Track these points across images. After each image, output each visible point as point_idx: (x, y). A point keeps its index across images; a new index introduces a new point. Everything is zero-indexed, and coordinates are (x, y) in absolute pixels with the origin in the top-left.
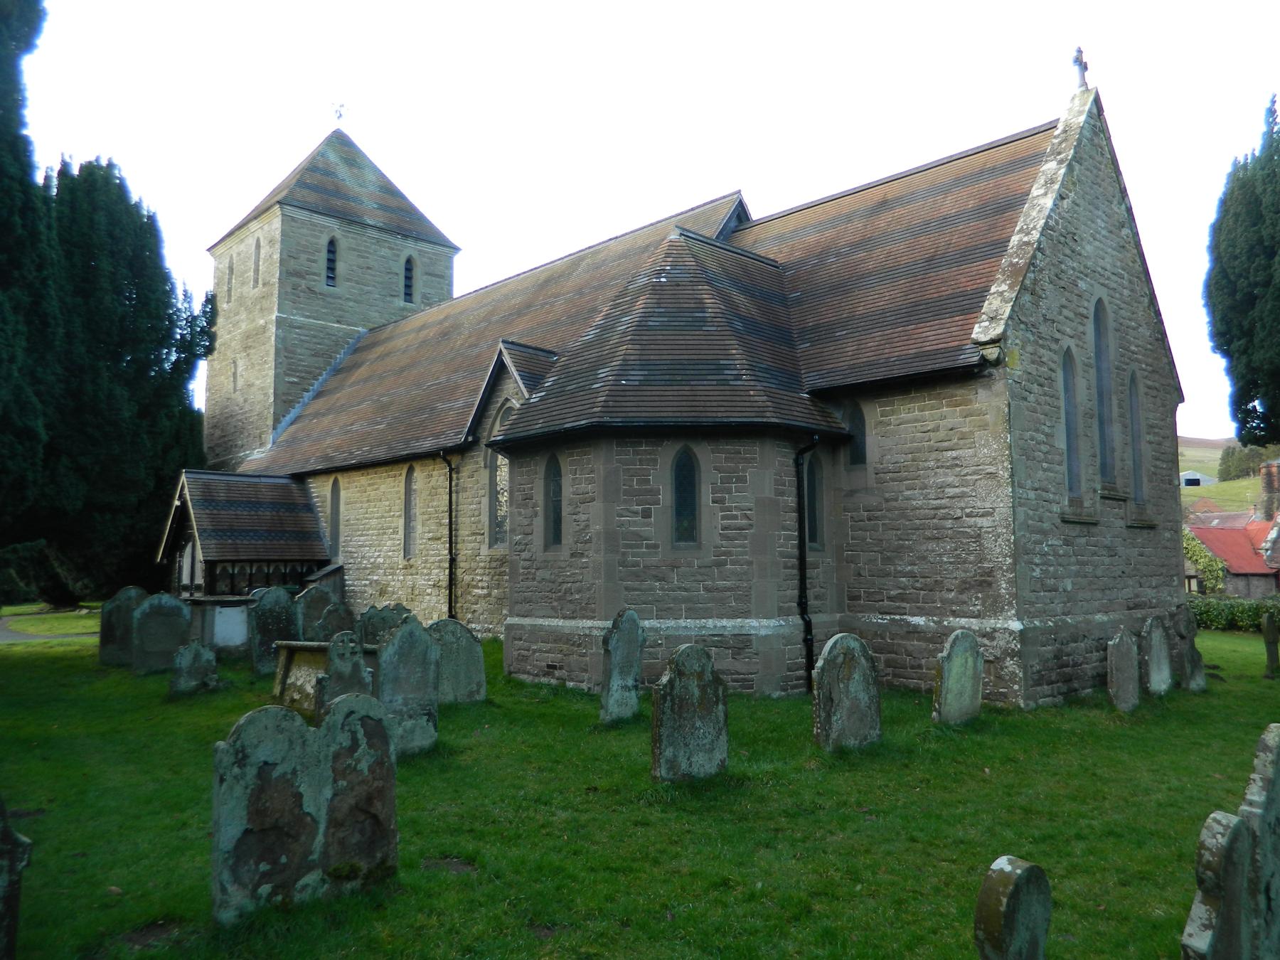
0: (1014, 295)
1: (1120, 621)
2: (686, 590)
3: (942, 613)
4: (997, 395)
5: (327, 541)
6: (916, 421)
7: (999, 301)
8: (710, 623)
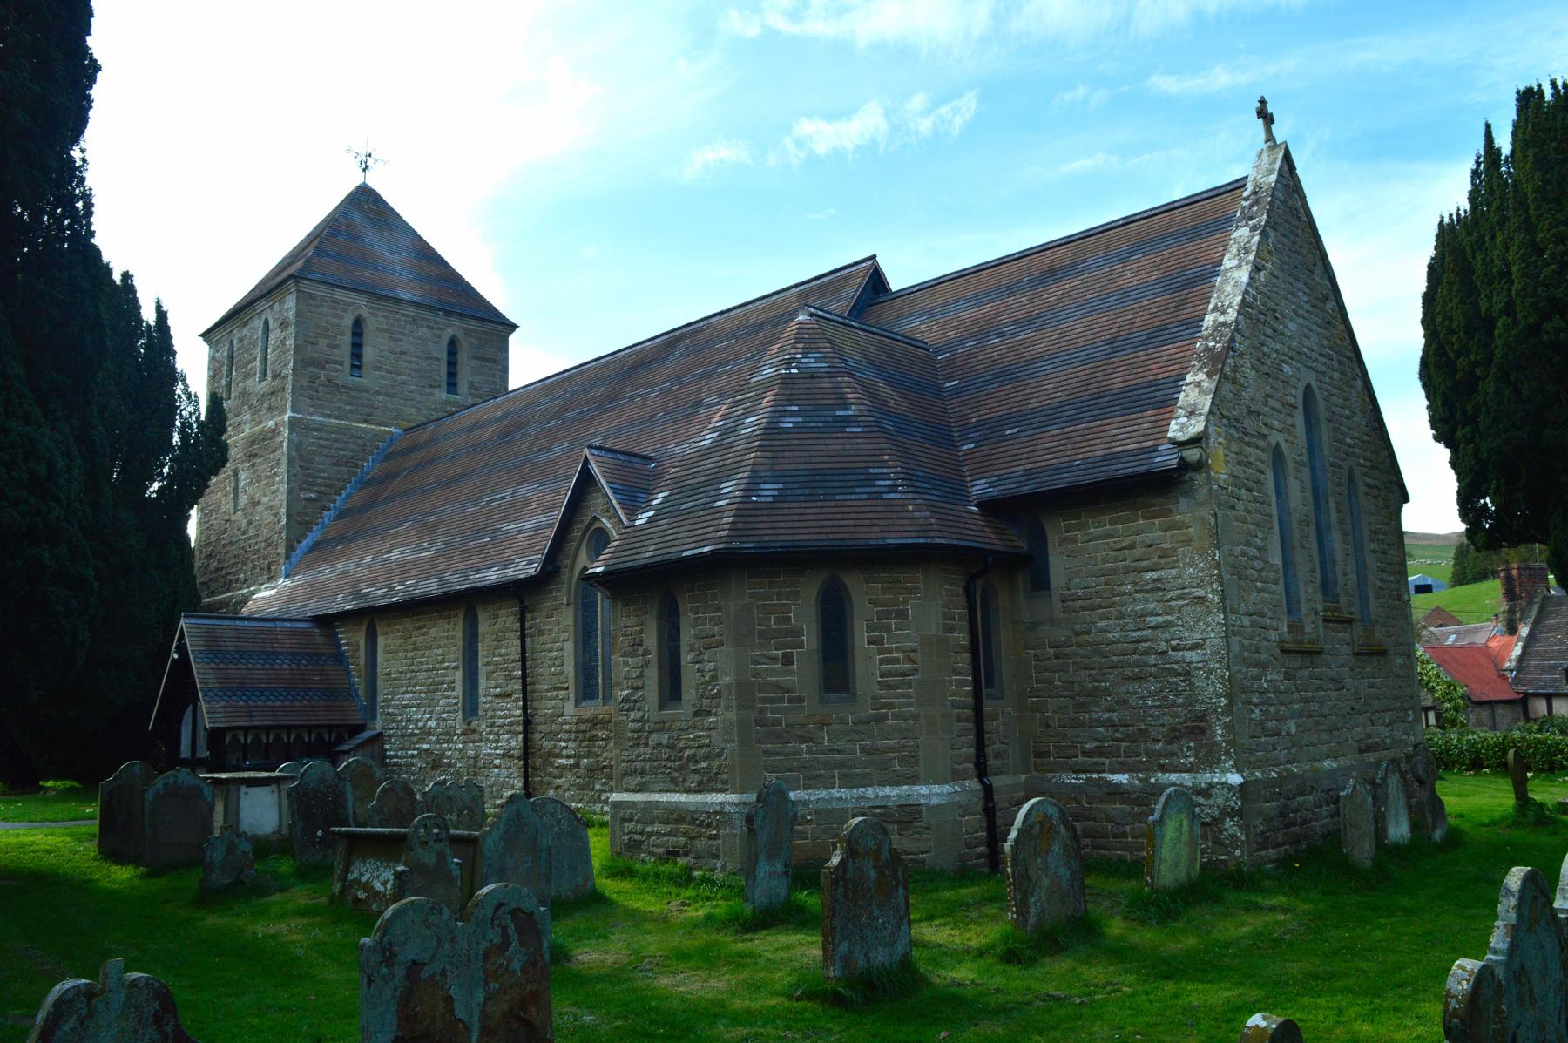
0: (1213, 386)
1: (1351, 768)
2: (839, 752)
3: (1148, 769)
4: (1201, 505)
6: (1109, 536)
7: (1196, 393)
8: (870, 792)
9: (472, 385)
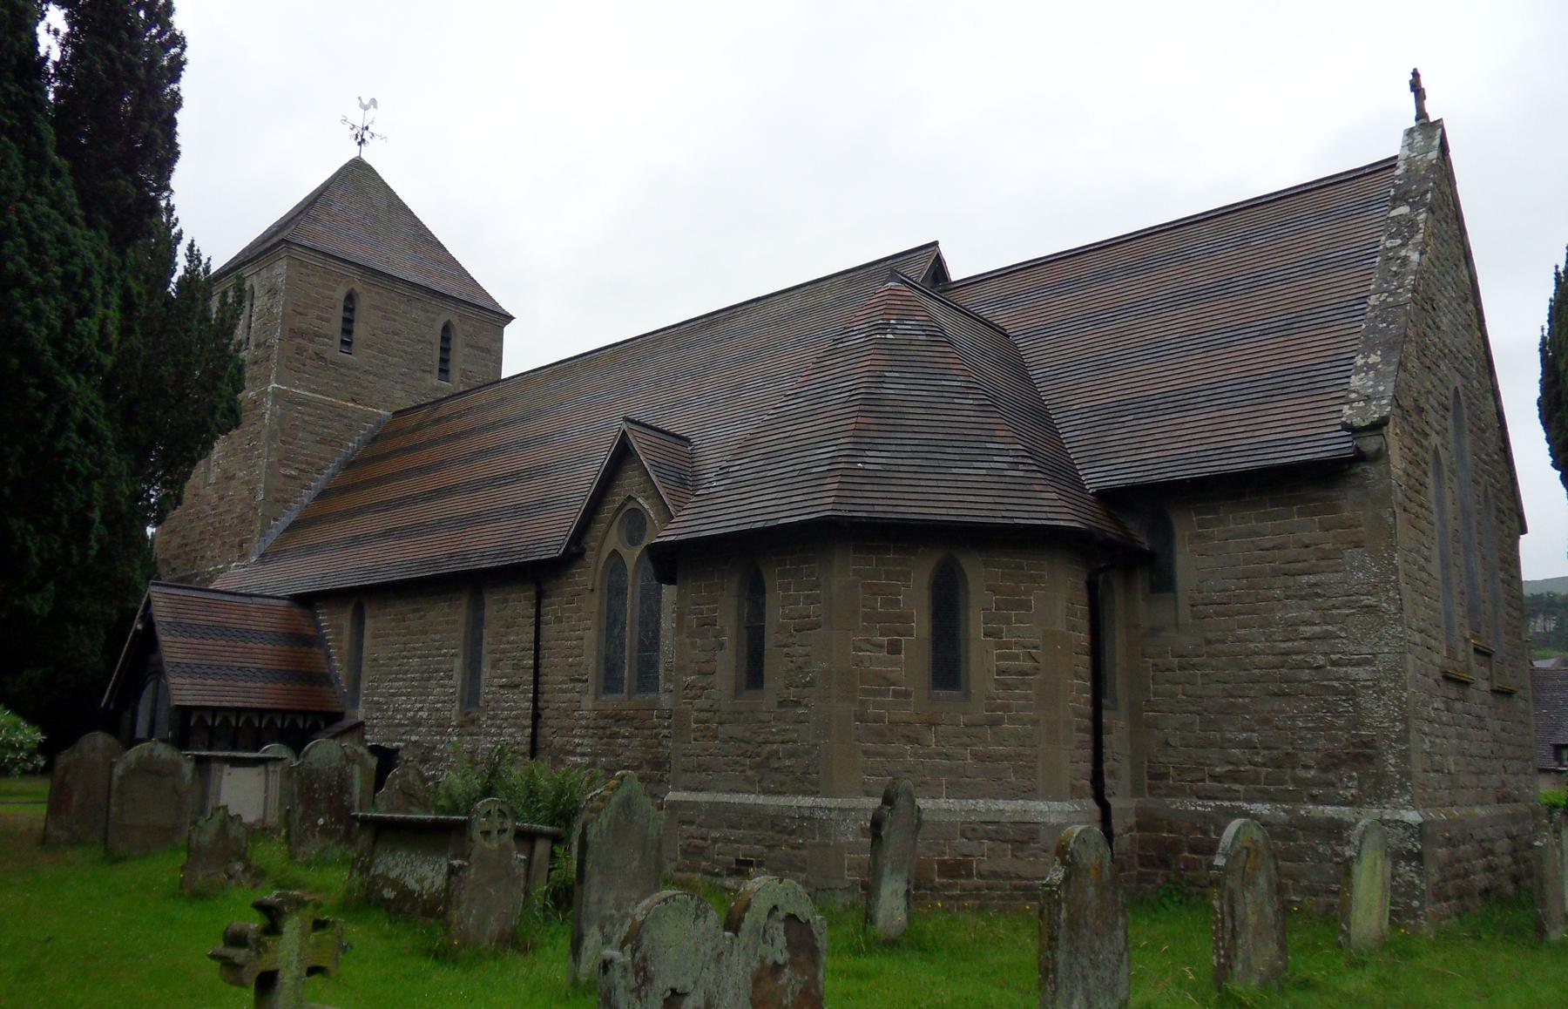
2: (948, 757)
3: (1294, 798)
5: (344, 686)
9: (464, 372)
